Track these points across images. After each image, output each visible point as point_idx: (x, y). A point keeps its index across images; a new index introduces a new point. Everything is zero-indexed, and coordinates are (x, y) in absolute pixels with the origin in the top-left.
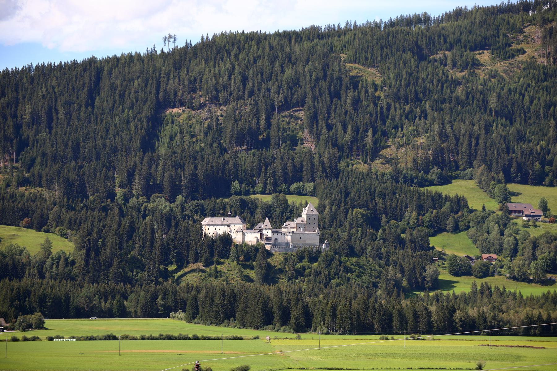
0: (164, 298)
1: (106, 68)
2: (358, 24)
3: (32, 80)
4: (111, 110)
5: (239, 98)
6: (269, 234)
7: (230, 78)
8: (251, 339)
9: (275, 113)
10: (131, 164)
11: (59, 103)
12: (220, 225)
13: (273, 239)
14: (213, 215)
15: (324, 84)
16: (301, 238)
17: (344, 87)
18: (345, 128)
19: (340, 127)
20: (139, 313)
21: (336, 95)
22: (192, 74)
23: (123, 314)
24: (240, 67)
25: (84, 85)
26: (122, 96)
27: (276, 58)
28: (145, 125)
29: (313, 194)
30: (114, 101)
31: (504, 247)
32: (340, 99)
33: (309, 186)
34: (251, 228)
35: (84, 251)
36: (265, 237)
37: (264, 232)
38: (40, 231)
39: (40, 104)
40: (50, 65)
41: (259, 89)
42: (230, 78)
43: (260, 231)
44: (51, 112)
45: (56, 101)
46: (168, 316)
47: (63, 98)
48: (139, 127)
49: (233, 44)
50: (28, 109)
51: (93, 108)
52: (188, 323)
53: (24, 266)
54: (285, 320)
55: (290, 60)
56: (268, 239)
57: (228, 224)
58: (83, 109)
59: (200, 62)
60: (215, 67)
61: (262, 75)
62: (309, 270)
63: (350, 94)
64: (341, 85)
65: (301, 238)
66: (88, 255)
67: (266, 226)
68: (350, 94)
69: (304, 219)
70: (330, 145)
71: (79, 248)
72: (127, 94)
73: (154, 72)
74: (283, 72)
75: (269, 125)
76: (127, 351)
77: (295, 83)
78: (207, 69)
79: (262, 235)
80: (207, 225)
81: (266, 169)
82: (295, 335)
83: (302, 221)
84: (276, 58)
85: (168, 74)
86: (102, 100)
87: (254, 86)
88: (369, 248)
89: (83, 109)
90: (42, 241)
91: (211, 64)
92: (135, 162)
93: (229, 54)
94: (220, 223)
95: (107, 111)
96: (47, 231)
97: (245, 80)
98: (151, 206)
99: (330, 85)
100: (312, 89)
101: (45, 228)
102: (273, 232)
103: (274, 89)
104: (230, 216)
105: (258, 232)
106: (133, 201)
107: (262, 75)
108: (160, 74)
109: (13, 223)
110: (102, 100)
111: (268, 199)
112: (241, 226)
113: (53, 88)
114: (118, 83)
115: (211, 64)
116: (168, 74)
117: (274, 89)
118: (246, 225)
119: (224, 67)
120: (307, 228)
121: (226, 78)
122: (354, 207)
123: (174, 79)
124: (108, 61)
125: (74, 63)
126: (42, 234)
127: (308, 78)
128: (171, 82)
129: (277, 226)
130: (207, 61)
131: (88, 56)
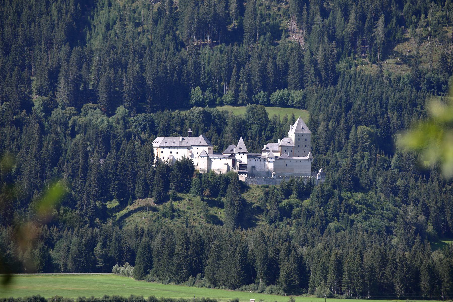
0: (104, 246)
10: (52, 62)
12: (177, 148)
13: (249, 167)
14: (166, 134)
16: (286, 165)
18: (346, 15)
29: (302, 106)
36: (238, 163)
37: (238, 157)
43: (232, 156)
48: (64, 10)
52: (139, 280)
57: (188, 145)
65: (286, 165)
67: (240, 148)
69: (291, 140)
70: (326, 38)
79: (234, 161)
80: (161, 147)
81: (238, 70)
83: (289, 143)
92: (59, 59)
94: (177, 144)
102: (249, 157)
104: (190, 135)
105: (230, 156)
106: (56, 114)
112: (206, 149)
118: (212, 147)
120: (296, 152)
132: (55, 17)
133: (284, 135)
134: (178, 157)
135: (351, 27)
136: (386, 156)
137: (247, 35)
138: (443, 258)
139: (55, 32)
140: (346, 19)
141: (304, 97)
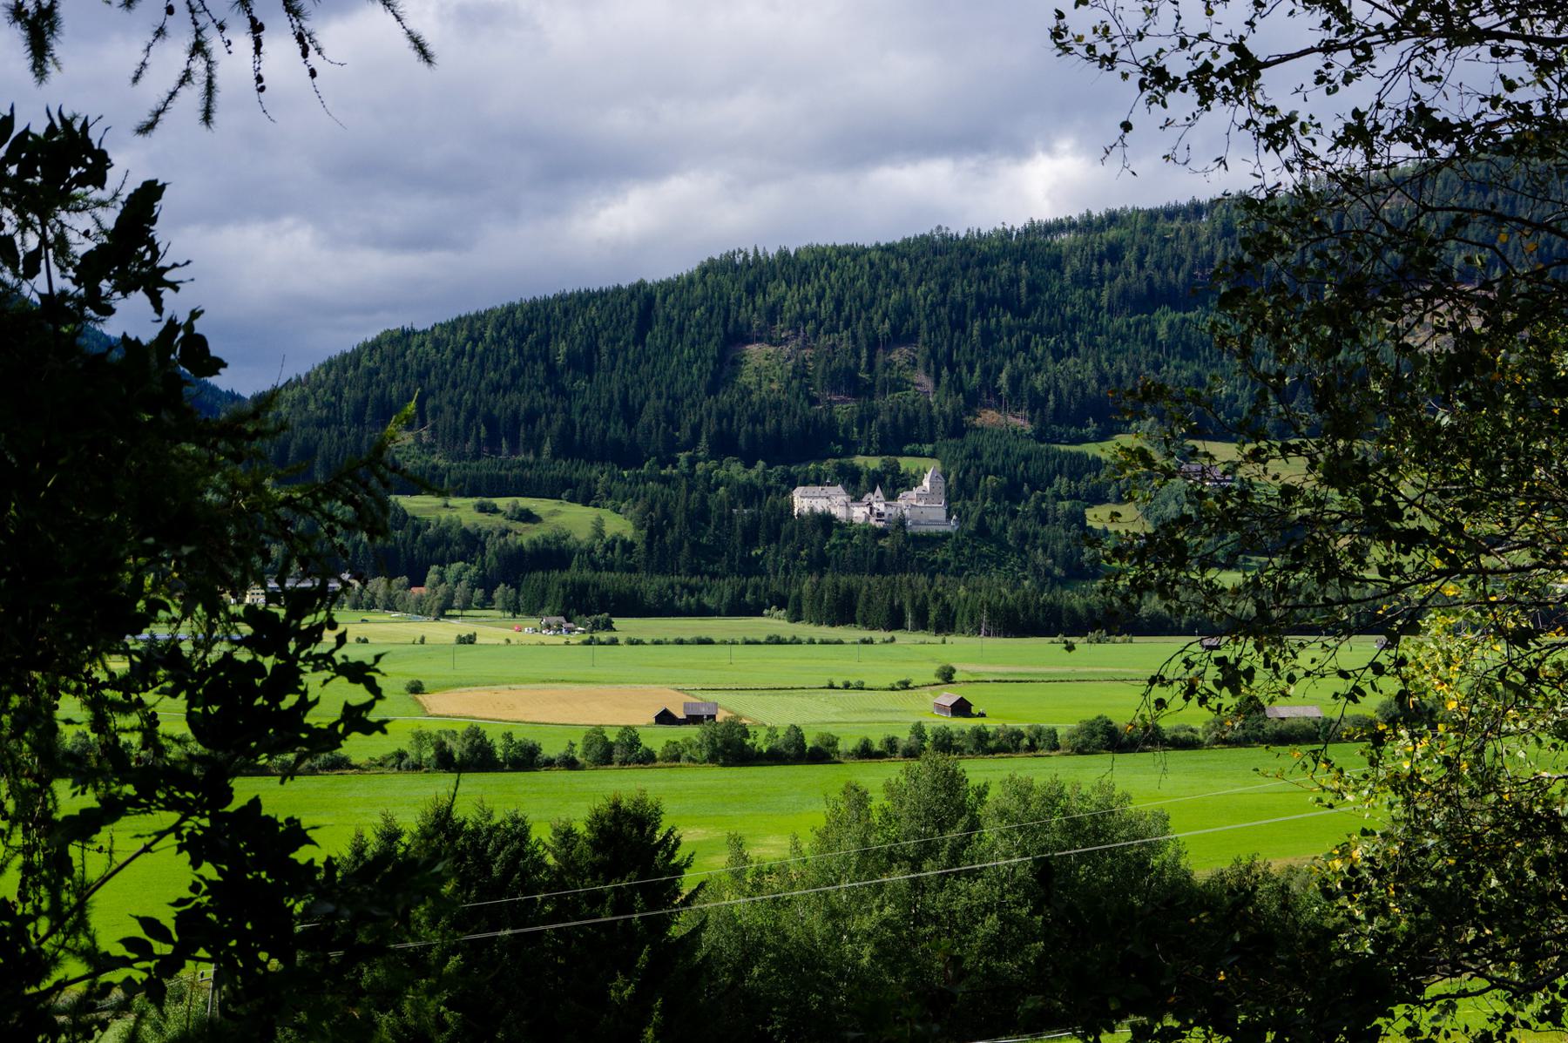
0: (754, 593)
1: (658, 295)
2: (983, 232)
3: (566, 312)
4: (668, 347)
5: (834, 329)
6: (882, 508)
7: (819, 305)
8: (855, 643)
9: (880, 351)
11: (601, 341)
14: (805, 484)
15: (943, 311)
17: (968, 315)
18: (971, 370)
19: (965, 370)
20: (723, 611)
21: (959, 325)
22: (771, 300)
23: (703, 611)
24: (832, 288)
25: (632, 313)
26: (681, 331)
27: (878, 277)
28: (711, 368)
29: (933, 455)
30: (670, 336)
31: (971, 783)
32: (964, 331)
33: (928, 448)
34: (857, 499)
35: (644, 532)
37: (875, 505)
38: (587, 505)
39: (578, 341)
40: (587, 291)
41: (859, 318)
42: (819, 305)
43: (870, 504)
44: (592, 349)
45: (597, 338)
46: (761, 615)
47: (605, 334)
49: (823, 261)
50: (563, 348)
51: (644, 347)
52: (795, 621)
53: (571, 553)
54: (921, 624)
55: (896, 281)
56: (880, 515)
58: (632, 348)
59: (780, 285)
60: (798, 290)
61: (861, 300)
62: (1363, 917)
63: (977, 324)
64: (965, 312)
66: (651, 535)
68: (977, 324)
71: (639, 527)
72: (686, 327)
73: (721, 298)
74: (888, 296)
75: (871, 366)
76: (1090, 669)
77: (905, 311)
78: (790, 294)
79: (871, 509)
82: (939, 639)
84: (878, 277)
85: (739, 300)
86: (654, 337)
87: (851, 314)
88: (1010, 528)
89: (632, 348)
90: (593, 518)
91: (795, 287)
92: (701, 416)
93: (817, 274)
95: (662, 350)
96: (596, 506)
97: (839, 303)
98: (722, 473)
99: (951, 312)
100: (927, 317)
101: (593, 502)
103: (876, 319)
104: (829, 485)
106: (700, 466)
107: (861, 300)
108: (729, 299)
109: (554, 495)
110: (654, 337)
111: (874, 463)
113: (593, 320)
114: (675, 312)
115: (795, 287)
116: (739, 300)
117: (876, 319)
119: (809, 291)
121: (814, 304)
122: (987, 473)
123: (747, 305)
124: (661, 284)
125: (618, 289)
126: (590, 509)
127: (922, 302)
128: (743, 310)
129: (891, 497)
130: (789, 285)
131: (635, 280)
132: (695, 378)
133: (918, 483)
134: (819, 509)
135: (977, 378)
136: (1122, 561)
137: (878, 389)
138: (170, 756)
139: (1555, 746)
140: (972, 375)
141: (935, 449)
